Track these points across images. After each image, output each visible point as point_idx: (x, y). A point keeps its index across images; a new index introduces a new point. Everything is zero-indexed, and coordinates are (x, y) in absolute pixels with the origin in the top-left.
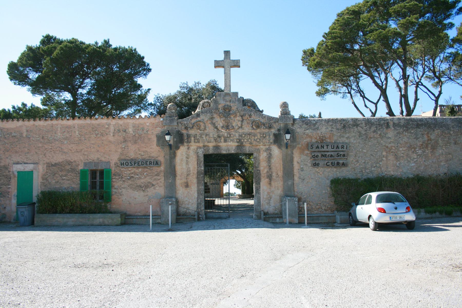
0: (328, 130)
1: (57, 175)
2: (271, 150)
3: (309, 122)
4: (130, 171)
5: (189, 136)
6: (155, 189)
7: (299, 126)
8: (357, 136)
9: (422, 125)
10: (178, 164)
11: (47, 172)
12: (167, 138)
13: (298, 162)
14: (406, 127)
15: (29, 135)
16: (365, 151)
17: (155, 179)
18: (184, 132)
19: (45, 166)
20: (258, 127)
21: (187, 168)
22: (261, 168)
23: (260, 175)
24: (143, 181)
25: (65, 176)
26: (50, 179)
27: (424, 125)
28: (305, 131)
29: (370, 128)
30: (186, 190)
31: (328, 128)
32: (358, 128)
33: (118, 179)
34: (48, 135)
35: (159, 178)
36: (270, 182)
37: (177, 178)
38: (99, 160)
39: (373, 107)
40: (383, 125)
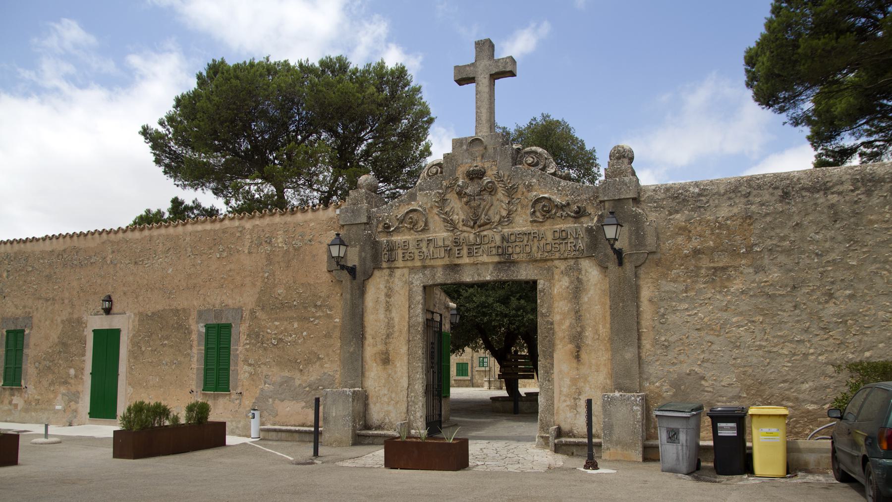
1: (154, 337)
2: (579, 271)
3: (680, 191)
4: (277, 327)
5: (391, 249)
11: (139, 331)
18: (383, 239)
22: (557, 318)
25: (167, 338)
28: (671, 217)
29: (869, 193)
32: (830, 197)
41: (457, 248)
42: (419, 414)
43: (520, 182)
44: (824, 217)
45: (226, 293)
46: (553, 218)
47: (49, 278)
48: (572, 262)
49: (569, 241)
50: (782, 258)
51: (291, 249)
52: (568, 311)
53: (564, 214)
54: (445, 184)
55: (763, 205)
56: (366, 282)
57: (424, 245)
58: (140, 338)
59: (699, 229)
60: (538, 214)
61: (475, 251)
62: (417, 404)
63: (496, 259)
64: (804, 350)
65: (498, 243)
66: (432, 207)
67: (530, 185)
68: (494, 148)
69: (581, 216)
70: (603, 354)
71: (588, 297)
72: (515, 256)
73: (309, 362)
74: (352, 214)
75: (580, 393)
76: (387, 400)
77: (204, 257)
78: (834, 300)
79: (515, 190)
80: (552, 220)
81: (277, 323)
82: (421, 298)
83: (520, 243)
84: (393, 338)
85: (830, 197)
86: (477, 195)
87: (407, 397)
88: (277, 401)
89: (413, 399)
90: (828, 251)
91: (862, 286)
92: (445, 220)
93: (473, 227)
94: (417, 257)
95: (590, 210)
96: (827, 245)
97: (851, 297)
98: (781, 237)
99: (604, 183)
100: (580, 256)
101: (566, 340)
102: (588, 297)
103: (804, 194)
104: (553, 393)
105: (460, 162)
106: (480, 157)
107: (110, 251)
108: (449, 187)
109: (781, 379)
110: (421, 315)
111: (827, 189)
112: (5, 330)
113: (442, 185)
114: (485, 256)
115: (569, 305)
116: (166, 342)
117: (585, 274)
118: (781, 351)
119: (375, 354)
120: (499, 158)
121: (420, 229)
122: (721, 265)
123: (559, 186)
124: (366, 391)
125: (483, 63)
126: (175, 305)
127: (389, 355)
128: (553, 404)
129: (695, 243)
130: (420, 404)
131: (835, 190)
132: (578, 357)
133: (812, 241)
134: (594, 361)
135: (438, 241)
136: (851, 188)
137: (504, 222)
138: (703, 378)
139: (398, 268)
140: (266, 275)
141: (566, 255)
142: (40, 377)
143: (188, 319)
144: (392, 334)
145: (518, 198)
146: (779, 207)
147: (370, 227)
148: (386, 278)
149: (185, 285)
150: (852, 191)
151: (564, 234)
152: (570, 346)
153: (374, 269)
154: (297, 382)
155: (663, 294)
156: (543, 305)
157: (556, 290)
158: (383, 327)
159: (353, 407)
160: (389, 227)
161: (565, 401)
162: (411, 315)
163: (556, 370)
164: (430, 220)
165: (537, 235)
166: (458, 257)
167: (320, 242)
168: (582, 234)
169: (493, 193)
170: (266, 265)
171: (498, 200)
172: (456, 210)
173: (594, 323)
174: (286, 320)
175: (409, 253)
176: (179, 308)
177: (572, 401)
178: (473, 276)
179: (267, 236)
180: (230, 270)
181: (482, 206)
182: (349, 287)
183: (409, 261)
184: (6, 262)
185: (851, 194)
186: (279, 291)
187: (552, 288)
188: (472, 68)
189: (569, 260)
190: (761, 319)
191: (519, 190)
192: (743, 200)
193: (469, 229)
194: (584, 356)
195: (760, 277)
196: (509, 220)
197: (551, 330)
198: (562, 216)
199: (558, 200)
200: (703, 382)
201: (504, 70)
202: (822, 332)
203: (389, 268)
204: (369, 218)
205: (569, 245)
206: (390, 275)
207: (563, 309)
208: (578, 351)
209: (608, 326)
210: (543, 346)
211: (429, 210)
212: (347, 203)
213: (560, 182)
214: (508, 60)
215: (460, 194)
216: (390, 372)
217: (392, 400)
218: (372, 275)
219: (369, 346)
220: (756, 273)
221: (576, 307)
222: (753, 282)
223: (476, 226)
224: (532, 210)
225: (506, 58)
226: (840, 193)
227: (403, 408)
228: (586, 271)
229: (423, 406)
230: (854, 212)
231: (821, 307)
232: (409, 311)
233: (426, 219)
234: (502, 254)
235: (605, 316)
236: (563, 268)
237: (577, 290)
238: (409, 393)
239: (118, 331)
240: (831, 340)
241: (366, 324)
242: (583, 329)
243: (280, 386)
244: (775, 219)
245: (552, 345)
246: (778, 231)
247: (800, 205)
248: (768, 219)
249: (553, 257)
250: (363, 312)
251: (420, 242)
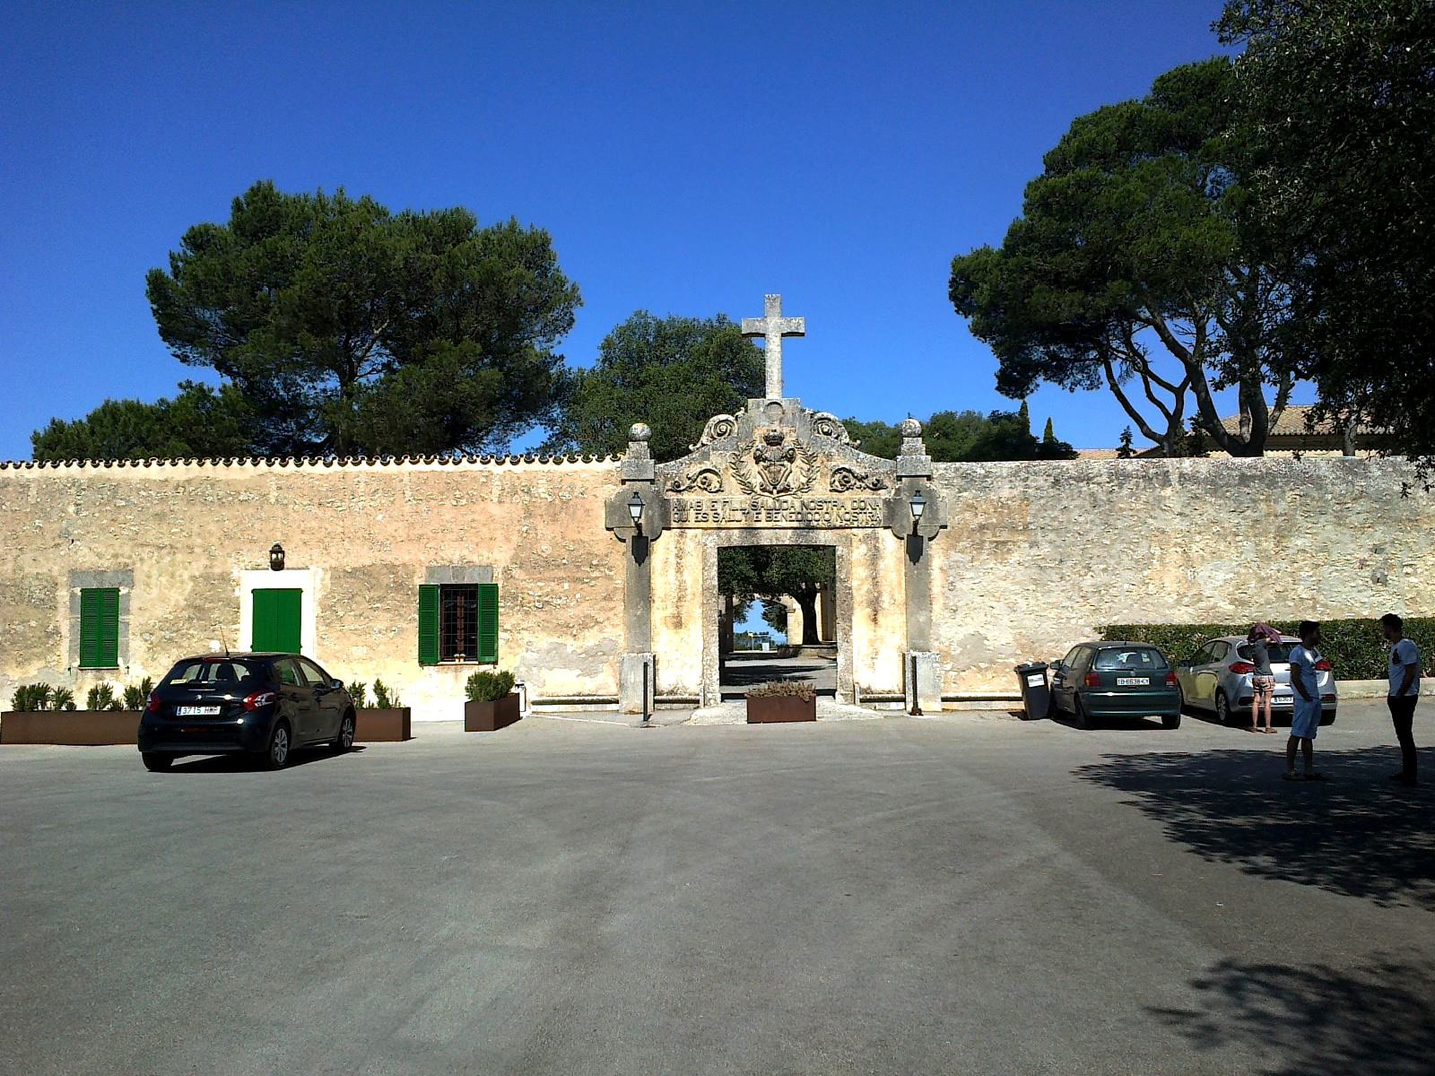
0: (1015, 492)
1: (358, 599)
2: (877, 539)
3: (969, 472)
4: (541, 588)
5: (682, 508)
6: (601, 631)
7: (946, 482)
8: (1088, 507)
9: (1253, 477)
10: (656, 572)
11: (332, 591)
12: (635, 511)
13: (941, 569)
14: (1213, 483)
15: (285, 498)
16: (1108, 542)
17: (602, 609)
18: (672, 496)
19: (329, 575)
20: (846, 486)
21: (678, 583)
22: (855, 584)
23: (852, 598)
24: (572, 613)
25: (381, 600)
26: (340, 609)
27: (1259, 480)
28: (960, 495)
29: (1121, 486)
30: (677, 633)
31: (1015, 486)
32: (1091, 486)
33: (512, 608)
34: (333, 500)
35: (611, 604)
36: (875, 615)
37: (655, 606)
38: (465, 561)
39: (1169, 401)
40: (1155, 480)
44: (1087, 502)
45: (467, 548)
47: (160, 517)
50: (1052, 536)
51: (557, 502)
55: (1038, 489)
58: (335, 600)
59: (984, 507)
64: (1068, 614)
65: (798, 510)
66: (727, 468)
73: (584, 626)
77: (433, 503)
78: (1091, 573)
81: (540, 584)
85: (1091, 486)
88: (544, 671)
90: (1087, 532)
91: (1112, 562)
92: (742, 483)
94: (711, 518)
95: (887, 483)
96: (1088, 526)
97: (1105, 570)
98: (1052, 518)
101: (864, 604)
103: (1072, 482)
105: (757, 424)
107: (274, 487)
109: (1050, 639)
111: (1089, 479)
112: (79, 589)
116: (378, 605)
118: (1050, 615)
122: (1002, 539)
126: (390, 558)
129: (981, 519)
131: (1095, 480)
132: (875, 620)
133: (1076, 522)
136: (1108, 480)
138: (986, 638)
140: (525, 529)
141: (864, 524)
142: (154, 652)
143: (412, 577)
146: (1052, 492)
149: (405, 536)
150: (1108, 482)
154: (569, 649)
155: (952, 563)
160: (679, 486)
167: (595, 495)
170: (525, 518)
174: (554, 581)
176: (397, 563)
178: (771, 540)
179: (523, 484)
180: (473, 521)
181: (782, 472)
184: (73, 491)
185: (1107, 485)
186: (543, 548)
190: (1034, 587)
192: (1022, 484)
194: (880, 618)
195: (1034, 551)
197: (849, 595)
199: (858, 471)
200: (985, 642)
202: (1081, 600)
208: (875, 615)
209: (904, 592)
212: (627, 456)
213: (859, 454)
215: (758, 459)
218: (660, 536)
220: (1031, 547)
222: (1028, 556)
226: (1099, 484)
230: (1109, 500)
231: (1081, 578)
236: (861, 536)
237: (874, 557)
239: (298, 592)
240: (1088, 606)
242: (880, 593)
243: (548, 653)
244: (1048, 502)
245: (851, 609)
246: (1049, 512)
247: (1068, 491)
248: (1042, 501)
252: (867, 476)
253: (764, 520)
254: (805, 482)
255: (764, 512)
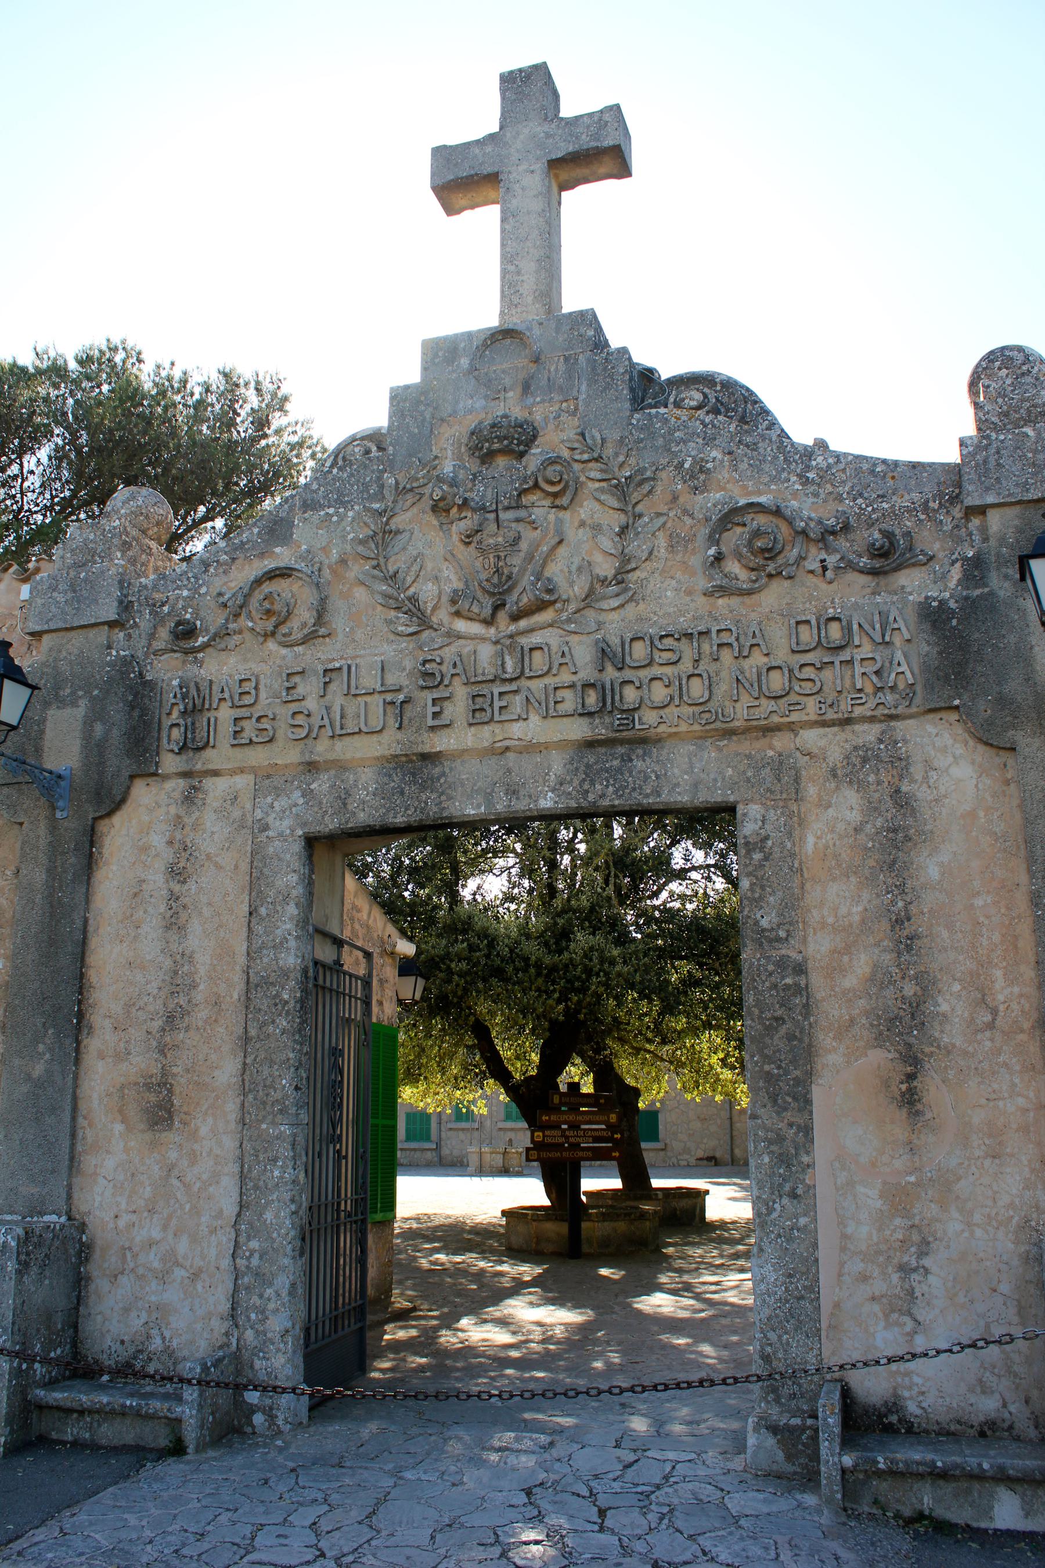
2: (900, 764)
21: (168, 963)
37: (93, 1045)
41: (429, 696)
42: (277, 1324)
43: (664, 461)
46: (790, 578)
48: (868, 734)
49: (858, 657)
52: (863, 921)
53: (832, 560)
54: (392, 481)
56: (103, 826)
57: (309, 688)
60: (733, 567)
61: (497, 704)
62: (271, 1284)
63: (578, 730)
65: (588, 673)
67: (700, 467)
68: (567, 359)
69: (897, 569)
70: (1014, 1085)
71: (941, 865)
72: (650, 717)
74: (70, 595)
75: (924, 1248)
76: (156, 1264)
79: (646, 487)
80: (787, 583)
82: (293, 878)
83: (669, 670)
84: (187, 1029)
86: (507, 508)
87: (234, 1256)
89: (255, 1261)
93: (489, 622)
94: (283, 732)
95: (929, 541)
99: (978, 448)
100: (900, 710)
102: (941, 865)
104: (815, 1246)
106: (519, 390)
108: (406, 491)
110: (292, 943)
113: (382, 486)
114: (534, 719)
115: (866, 895)
117: (926, 778)
119: (123, 1087)
120: (584, 388)
121: (300, 636)
123: (808, 468)
124: (82, 1227)
125: (526, 131)
127: (170, 1091)
128: (813, 1287)
130: (283, 1282)
134: (977, 1118)
135: (363, 671)
137: (604, 598)
139: (216, 773)
141: (845, 705)
144: (185, 1013)
145: (659, 515)
147: (129, 637)
148: (173, 810)
151: (835, 631)
152: (879, 1058)
153: (132, 777)
156: (761, 898)
157: (811, 840)
158: (153, 988)
159: (19, 1293)
161: (864, 1278)
162: (257, 943)
163: (822, 1149)
164: (337, 605)
165: (731, 640)
166: (432, 728)
168: (906, 626)
169: (564, 501)
171: (582, 524)
172: (429, 565)
173: (971, 965)
175: (259, 719)
177: (895, 1277)
181: (524, 545)
182: (43, 843)
183: (259, 748)
187: (796, 833)
188: (489, 149)
189: (857, 728)
191: (659, 489)
193: (475, 628)
196: (626, 590)
198: (825, 569)
201: (593, 144)
203: (186, 775)
204: (125, 606)
205: (858, 669)
206: (189, 799)
207: (843, 910)
208: (911, 1077)
209: (1029, 973)
210: (767, 1059)
211: (334, 572)
214: (607, 117)
216: (173, 1155)
217: (177, 1264)
218: (123, 801)
219: (101, 1056)
221: (893, 902)
223: (502, 616)
224: (712, 551)
225: (601, 111)
227: (219, 1300)
228: (929, 766)
229: (292, 1293)
232: (250, 929)
233: (323, 601)
234: (600, 711)
235: (1016, 938)
236: (835, 756)
238: (242, 1239)
241: (93, 976)
242: (927, 984)
249: (794, 717)
250: (85, 932)
251: (297, 679)
252: (846, 528)
253: (461, 721)
254: (610, 573)
255: (461, 692)
